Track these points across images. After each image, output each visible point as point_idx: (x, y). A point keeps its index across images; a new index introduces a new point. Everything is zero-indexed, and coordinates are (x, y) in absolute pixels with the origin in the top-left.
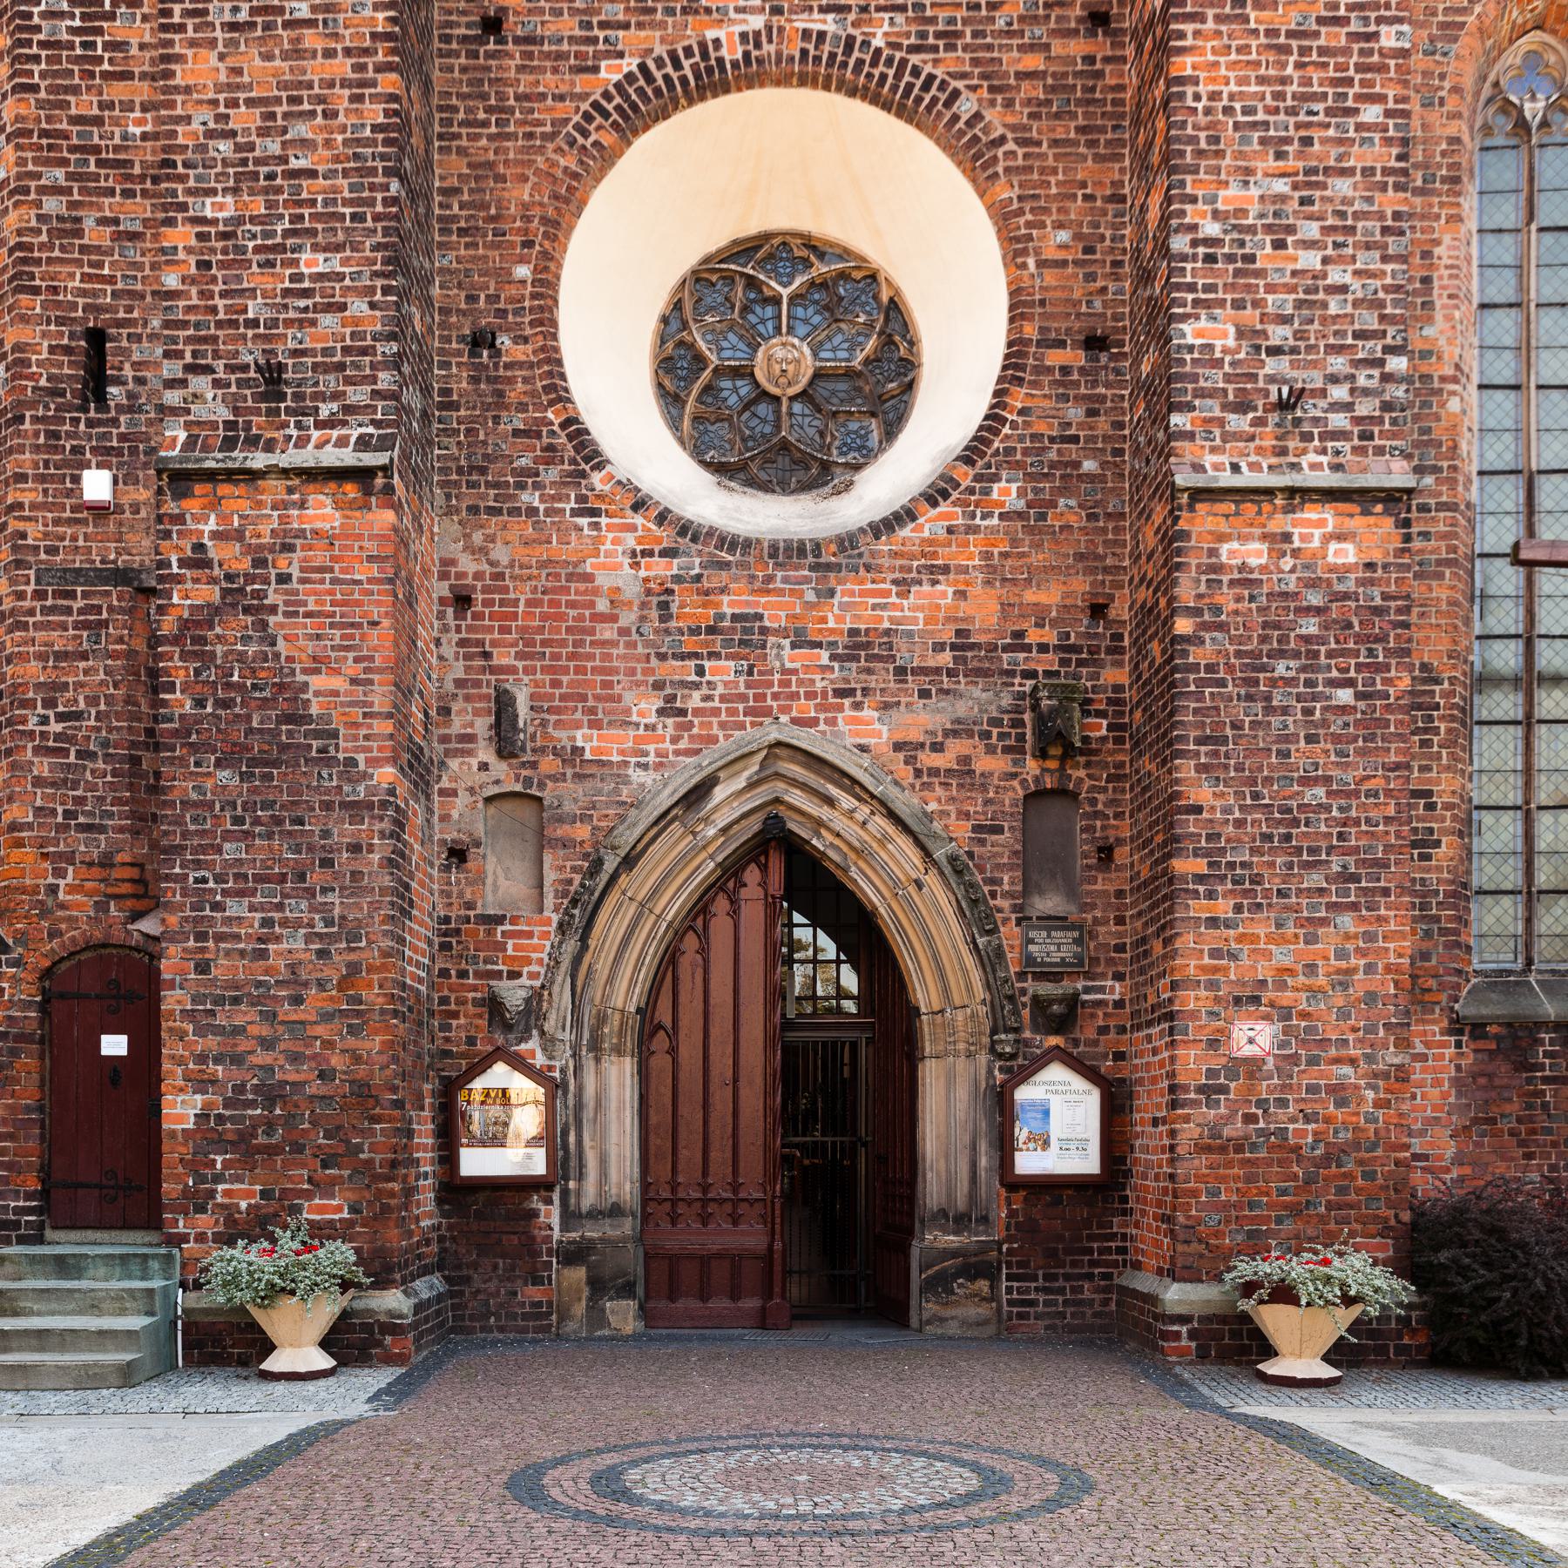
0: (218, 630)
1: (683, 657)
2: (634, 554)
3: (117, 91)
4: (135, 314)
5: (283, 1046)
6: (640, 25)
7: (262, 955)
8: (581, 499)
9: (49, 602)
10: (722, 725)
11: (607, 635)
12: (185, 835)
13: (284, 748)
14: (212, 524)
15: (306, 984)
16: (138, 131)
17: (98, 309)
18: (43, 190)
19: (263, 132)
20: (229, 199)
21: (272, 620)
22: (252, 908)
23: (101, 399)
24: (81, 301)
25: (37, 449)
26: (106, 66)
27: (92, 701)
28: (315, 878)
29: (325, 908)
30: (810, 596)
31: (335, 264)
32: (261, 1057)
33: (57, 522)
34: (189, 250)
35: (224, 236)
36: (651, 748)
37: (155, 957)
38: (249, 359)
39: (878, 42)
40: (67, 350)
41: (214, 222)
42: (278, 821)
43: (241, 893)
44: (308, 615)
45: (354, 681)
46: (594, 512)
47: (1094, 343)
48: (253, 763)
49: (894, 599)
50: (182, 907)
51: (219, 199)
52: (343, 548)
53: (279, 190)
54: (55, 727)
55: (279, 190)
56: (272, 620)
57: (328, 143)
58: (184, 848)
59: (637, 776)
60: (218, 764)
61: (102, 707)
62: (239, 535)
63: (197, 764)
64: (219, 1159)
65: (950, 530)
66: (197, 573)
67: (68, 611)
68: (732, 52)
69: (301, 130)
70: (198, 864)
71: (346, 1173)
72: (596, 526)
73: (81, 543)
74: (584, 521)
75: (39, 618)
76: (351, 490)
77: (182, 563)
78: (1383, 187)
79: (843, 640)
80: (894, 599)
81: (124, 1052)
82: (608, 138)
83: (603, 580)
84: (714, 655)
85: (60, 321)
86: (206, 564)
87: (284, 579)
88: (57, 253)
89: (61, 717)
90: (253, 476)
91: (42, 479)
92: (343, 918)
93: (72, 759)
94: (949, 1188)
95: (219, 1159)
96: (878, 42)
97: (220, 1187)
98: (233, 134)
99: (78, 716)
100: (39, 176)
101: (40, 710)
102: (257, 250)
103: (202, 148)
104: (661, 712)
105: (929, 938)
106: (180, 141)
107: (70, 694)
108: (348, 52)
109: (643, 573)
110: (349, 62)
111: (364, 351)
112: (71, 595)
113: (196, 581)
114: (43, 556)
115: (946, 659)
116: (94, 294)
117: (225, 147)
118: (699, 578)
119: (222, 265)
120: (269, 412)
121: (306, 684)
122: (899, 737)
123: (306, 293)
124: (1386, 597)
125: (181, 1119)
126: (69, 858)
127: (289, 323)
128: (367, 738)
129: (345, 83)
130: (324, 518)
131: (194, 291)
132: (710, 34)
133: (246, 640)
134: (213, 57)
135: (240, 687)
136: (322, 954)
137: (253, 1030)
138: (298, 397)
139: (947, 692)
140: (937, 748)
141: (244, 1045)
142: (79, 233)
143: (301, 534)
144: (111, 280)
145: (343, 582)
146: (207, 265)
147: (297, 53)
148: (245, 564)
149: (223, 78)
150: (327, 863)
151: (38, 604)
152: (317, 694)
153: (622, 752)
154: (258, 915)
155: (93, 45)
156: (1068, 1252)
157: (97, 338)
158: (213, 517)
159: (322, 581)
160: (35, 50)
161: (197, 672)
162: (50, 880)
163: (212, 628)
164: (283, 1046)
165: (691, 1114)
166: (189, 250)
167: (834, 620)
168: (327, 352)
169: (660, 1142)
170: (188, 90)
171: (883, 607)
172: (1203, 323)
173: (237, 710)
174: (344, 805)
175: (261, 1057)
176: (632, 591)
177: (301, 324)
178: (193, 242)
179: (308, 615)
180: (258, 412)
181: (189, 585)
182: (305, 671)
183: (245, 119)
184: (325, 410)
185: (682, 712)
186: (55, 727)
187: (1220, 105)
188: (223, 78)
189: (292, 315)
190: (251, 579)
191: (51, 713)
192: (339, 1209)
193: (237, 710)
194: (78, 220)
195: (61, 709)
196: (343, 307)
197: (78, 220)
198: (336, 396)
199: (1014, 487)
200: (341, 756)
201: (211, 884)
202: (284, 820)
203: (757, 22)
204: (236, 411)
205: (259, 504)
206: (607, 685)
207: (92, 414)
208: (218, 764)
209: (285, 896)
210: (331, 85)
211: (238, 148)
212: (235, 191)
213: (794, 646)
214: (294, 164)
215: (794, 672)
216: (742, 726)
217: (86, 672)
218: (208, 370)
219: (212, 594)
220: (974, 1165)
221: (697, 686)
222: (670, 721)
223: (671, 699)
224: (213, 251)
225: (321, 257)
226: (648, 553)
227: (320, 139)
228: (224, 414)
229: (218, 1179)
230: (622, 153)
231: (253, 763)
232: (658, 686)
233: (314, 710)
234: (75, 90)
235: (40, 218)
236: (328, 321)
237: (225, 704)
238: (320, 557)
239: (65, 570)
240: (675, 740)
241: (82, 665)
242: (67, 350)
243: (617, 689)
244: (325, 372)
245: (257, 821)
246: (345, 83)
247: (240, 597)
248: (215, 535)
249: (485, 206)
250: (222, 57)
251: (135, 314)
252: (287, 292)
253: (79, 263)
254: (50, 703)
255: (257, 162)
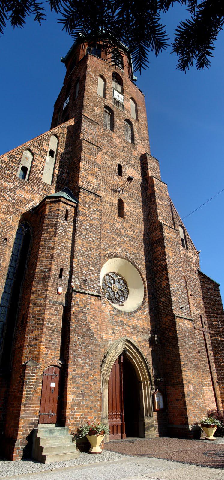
0: (79, 315)
1: (115, 325)
2: (109, 310)
3: (68, 240)
4: (67, 268)
5: (85, 386)
6: (110, 248)
7: (83, 369)
8: (103, 302)
9: (51, 306)
10: (120, 336)
11: (106, 321)
12: (73, 347)
13: (87, 334)
14: (79, 299)
15: (89, 375)
16: (69, 246)
17: (63, 266)
18: (57, 249)
19: (86, 251)
20: (82, 258)
21: (86, 314)
22: (82, 361)
23: (61, 278)
24: (60, 264)
25: (52, 283)
26: (66, 237)
27: (56, 322)
28: (91, 356)
29: (91, 361)
30: (128, 320)
31: (93, 269)
32: (82, 388)
33: (53, 294)
34: (77, 262)
35: (81, 262)
36: (111, 338)
37: (55, 191)
38: (83, 278)
39: (132, 257)
40: (58, 270)
41: (80, 260)
42: (86, 346)
43: (80, 358)
44: (91, 315)
45: (96, 325)
46: (105, 304)
47: (6, 239)
48: (83, 336)
49: (137, 322)
50: (72, 360)
51: (81, 257)
52: (95, 306)
53: (87, 258)
54: (50, 326)
55: (87, 258)
56: (86, 314)
57: (93, 255)
58: (72, 349)
59: (110, 342)
60: (78, 336)
61: (57, 324)
62: (82, 302)
63: (75, 335)
64: (75, 408)
65: (141, 314)
66: (77, 306)
67: (53, 307)
68: (119, 254)
69: (90, 252)
70: (75, 352)
71: (94, 410)
72: (105, 306)
73: (56, 297)
74: (104, 305)
75: (49, 308)
76: (96, 298)
77: (75, 304)
78: (43, 190)
79: (132, 326)
80: (137, 322)
81: (54, 386)
82: (107, 259)
83: (106, 313)
84: (118, 326)
85: (57, 266)
86: (78, 305)
87: (88, 309)
88: (58, 257)
89: (51, 324)
90: (85, 294)
91: (52, 287)
92: (94, 363)
93: (52, 332)
94: (22, 26)
95: (75, 408)
96: (132, 257)
97: (75, 414)
98: (83, 250)
99: (53, 324)
100: (57, 247)
101: (48, 323)
102: (85, 265)
103: (79, 251)
104: (113, 333)
105: (116, 344)
106: (77, 249)
107: (52, 321)
108: (96, 246)
109: (110, 313)
110: (96, 247)
111: (96, 280)
112: (54, 305)
113: (77, 307)
114: (51, 298)
115: (142, 330)
116: (62, 264)
117: (82, 251)
118: (116, 315)
119: (80, 265)
120: (85, 285)
121: (90, 325)
122: (139, 340)
123: (90, 271)
124: (217, 342)
125: (70, 400)
126: (50, 349)
127: (88, 275)
128: (97, 334)
129: (95, 249)
130: (93, 301)
131: (77, 267)
132: (117, 251)
133: (83, 317)
134: (81, 241)
135: (81, 324)
136: (91, 369)
137: (81, 383)
138: (88, 284)
139: (143, 335)
140: (142, 342)
141: (80, 386)
142: (61, 256)
143: (90, 303)
144: (64, 263)
145: (95, 311)
146: (79, 265)
147: (90, 244)
148: (126, 165)
149: (82, 244)
150: (92, 354)
151: (49, 306)
152: (91, 326)
153: (108, 338)
154: (83, 362)
155: (65, 234)
156: (32, 373)
157: (62, 270)
158: (79, 298)
159: (92, 310)
160: (58, 233)
161: (76, 321)
162: (47, 352)
163: (78, 314)
164: (85, 386)
165: (114, 400)
166: (77, 262)
167: (130, 323)
168: (92, 279)
169: (111, 400)
170: (78, 244)
171: (136, 322)
172: (174, 298)
173: (81, 327)
174: (94, 344)
175: (82, 388)
176: (109, 315)
177: (89, 275)
178: (77, 261)
179: (91, 315)
180: (83, 285)
181: (76, 307)
182: (90, 323)
183: (84, 249)
184: (92, 286)
185: (115, 333)
186: (50, 326)
187: (54, 220)
188: (82, 244)
189: (88, 274)
190: (84, 308)
191: (49, 323)
192: (93, 418)
193: (81, 327)
194: (61, 254)
195: (51, 323)
196: (94, 274)
197: (61, 254)
198: (93, 285)
199: (147, 310)
200: (94, 336)
201: (76, 356)
202: (86, 346)
203: (121, 252)
204: (80, 284)
205: (85, 298)
206: (106, 328)
207: (60, 279)
208: (78, 336)
209: (86, 359)
210: (94, 248)
211: (83, 252)
212: (83, 257)
213: (127, 326)
214: (89, 256)
215: (127, 329)
216: (122, 336)
217: (55, 318)
218: (78, 278)
219: (78, 309)
220: (2, 27)
221: (116, 330)
222: (113, 334)
223: (114, 331)
224: (79, 263)
225: (92, 268)
226: (111, 310)
227: (92, 254)
228: (79, 284)
229: (75, 412)
230: (190, 439)
231: (83, 336)
232: (112, 329)
233: (91, 329)
234: (63, 239)
235: (56, 252)
236: (92, 276)
237: (79, 326)
238: (92, 306)
239: (54, 301)
240: (114, 337)
241: (55, 316)
242: (58, 270)
243: (107, 329)
244: (92, 282)
245: (83, 346)
246: (95, 249)
247: (82, 311)
248: (79, 301)
249: (217, 364)
250: (82, 241)
251: (67, 268)
252: (88, 271)
253: (61, 259)
254: (49, 322)
255: (85, 254)
